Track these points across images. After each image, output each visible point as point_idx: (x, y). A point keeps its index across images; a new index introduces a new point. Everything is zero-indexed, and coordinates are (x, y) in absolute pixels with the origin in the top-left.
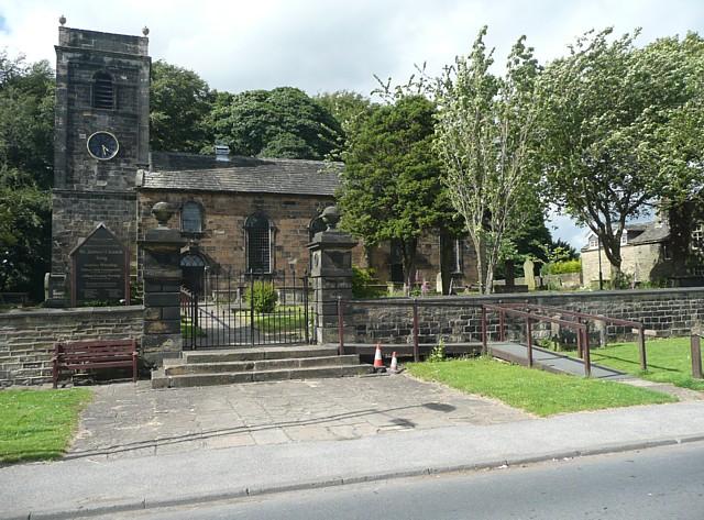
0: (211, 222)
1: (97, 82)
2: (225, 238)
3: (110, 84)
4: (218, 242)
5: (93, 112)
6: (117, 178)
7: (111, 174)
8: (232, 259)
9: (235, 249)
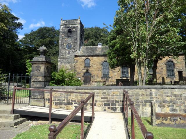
0: (92, 64)
1: (69, 32)
2: (96, 68)
3: (71, 31)
4: (94, 69)
5: (67, 38)
6: (72, 54)
7: (71, 53)
8: (98, 74)
9: (99, 71)
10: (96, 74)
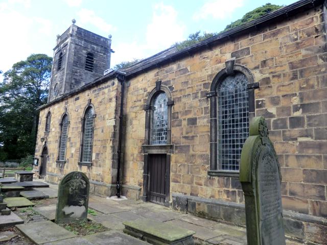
10: (138, 118)
